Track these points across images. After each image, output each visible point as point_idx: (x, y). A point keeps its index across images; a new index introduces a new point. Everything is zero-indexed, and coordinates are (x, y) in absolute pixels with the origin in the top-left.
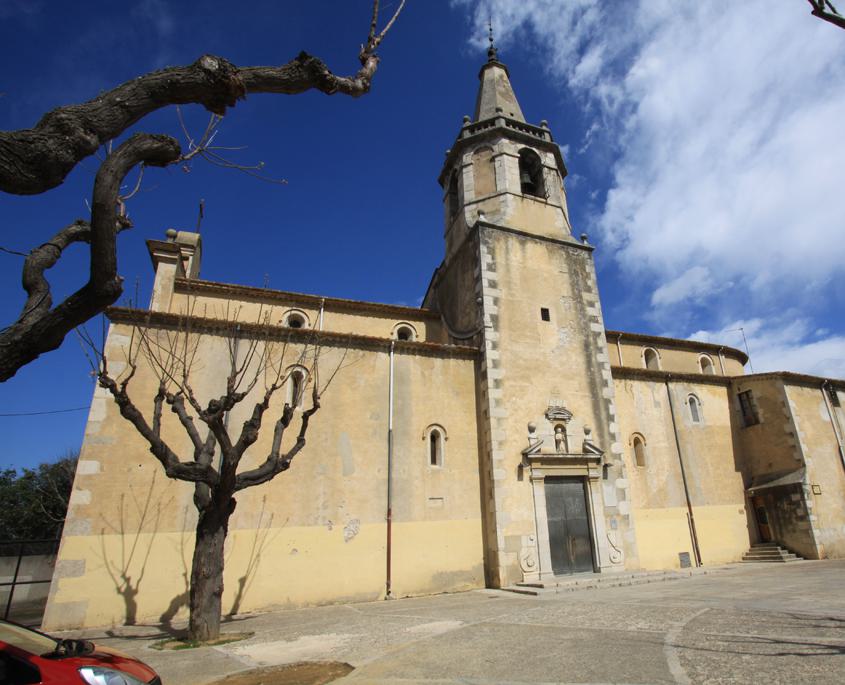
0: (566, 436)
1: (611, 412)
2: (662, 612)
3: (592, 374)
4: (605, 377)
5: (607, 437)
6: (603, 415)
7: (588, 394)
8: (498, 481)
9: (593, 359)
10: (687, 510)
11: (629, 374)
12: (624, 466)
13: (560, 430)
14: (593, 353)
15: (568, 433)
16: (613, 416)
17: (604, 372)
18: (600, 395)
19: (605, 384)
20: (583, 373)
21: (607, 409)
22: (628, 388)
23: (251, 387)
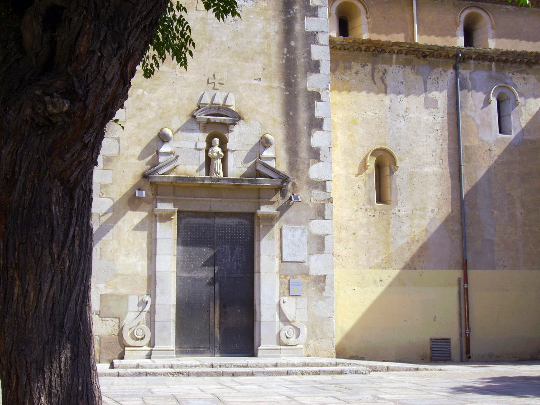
0: (225, 151)
1: (318, 114)
2: (107, 267)
3: (291, 50)
4: (315, 56)
5: (304, 154)
6: (303, 117)
7: (277, 84)
8: (174, 255)
9: (297, 27)
10: (458, 273)
11: (383, 51)
12: (330, 200)
13: (217, 141)
14: (299, 16)
15: (229, 146)
16: (322, 120)
17: (314, 49)
18: (301, 86)
19: (315, 67)
20: (274, 49)
21: (311, 108)
22: (377, 76)
23: (281, 395)
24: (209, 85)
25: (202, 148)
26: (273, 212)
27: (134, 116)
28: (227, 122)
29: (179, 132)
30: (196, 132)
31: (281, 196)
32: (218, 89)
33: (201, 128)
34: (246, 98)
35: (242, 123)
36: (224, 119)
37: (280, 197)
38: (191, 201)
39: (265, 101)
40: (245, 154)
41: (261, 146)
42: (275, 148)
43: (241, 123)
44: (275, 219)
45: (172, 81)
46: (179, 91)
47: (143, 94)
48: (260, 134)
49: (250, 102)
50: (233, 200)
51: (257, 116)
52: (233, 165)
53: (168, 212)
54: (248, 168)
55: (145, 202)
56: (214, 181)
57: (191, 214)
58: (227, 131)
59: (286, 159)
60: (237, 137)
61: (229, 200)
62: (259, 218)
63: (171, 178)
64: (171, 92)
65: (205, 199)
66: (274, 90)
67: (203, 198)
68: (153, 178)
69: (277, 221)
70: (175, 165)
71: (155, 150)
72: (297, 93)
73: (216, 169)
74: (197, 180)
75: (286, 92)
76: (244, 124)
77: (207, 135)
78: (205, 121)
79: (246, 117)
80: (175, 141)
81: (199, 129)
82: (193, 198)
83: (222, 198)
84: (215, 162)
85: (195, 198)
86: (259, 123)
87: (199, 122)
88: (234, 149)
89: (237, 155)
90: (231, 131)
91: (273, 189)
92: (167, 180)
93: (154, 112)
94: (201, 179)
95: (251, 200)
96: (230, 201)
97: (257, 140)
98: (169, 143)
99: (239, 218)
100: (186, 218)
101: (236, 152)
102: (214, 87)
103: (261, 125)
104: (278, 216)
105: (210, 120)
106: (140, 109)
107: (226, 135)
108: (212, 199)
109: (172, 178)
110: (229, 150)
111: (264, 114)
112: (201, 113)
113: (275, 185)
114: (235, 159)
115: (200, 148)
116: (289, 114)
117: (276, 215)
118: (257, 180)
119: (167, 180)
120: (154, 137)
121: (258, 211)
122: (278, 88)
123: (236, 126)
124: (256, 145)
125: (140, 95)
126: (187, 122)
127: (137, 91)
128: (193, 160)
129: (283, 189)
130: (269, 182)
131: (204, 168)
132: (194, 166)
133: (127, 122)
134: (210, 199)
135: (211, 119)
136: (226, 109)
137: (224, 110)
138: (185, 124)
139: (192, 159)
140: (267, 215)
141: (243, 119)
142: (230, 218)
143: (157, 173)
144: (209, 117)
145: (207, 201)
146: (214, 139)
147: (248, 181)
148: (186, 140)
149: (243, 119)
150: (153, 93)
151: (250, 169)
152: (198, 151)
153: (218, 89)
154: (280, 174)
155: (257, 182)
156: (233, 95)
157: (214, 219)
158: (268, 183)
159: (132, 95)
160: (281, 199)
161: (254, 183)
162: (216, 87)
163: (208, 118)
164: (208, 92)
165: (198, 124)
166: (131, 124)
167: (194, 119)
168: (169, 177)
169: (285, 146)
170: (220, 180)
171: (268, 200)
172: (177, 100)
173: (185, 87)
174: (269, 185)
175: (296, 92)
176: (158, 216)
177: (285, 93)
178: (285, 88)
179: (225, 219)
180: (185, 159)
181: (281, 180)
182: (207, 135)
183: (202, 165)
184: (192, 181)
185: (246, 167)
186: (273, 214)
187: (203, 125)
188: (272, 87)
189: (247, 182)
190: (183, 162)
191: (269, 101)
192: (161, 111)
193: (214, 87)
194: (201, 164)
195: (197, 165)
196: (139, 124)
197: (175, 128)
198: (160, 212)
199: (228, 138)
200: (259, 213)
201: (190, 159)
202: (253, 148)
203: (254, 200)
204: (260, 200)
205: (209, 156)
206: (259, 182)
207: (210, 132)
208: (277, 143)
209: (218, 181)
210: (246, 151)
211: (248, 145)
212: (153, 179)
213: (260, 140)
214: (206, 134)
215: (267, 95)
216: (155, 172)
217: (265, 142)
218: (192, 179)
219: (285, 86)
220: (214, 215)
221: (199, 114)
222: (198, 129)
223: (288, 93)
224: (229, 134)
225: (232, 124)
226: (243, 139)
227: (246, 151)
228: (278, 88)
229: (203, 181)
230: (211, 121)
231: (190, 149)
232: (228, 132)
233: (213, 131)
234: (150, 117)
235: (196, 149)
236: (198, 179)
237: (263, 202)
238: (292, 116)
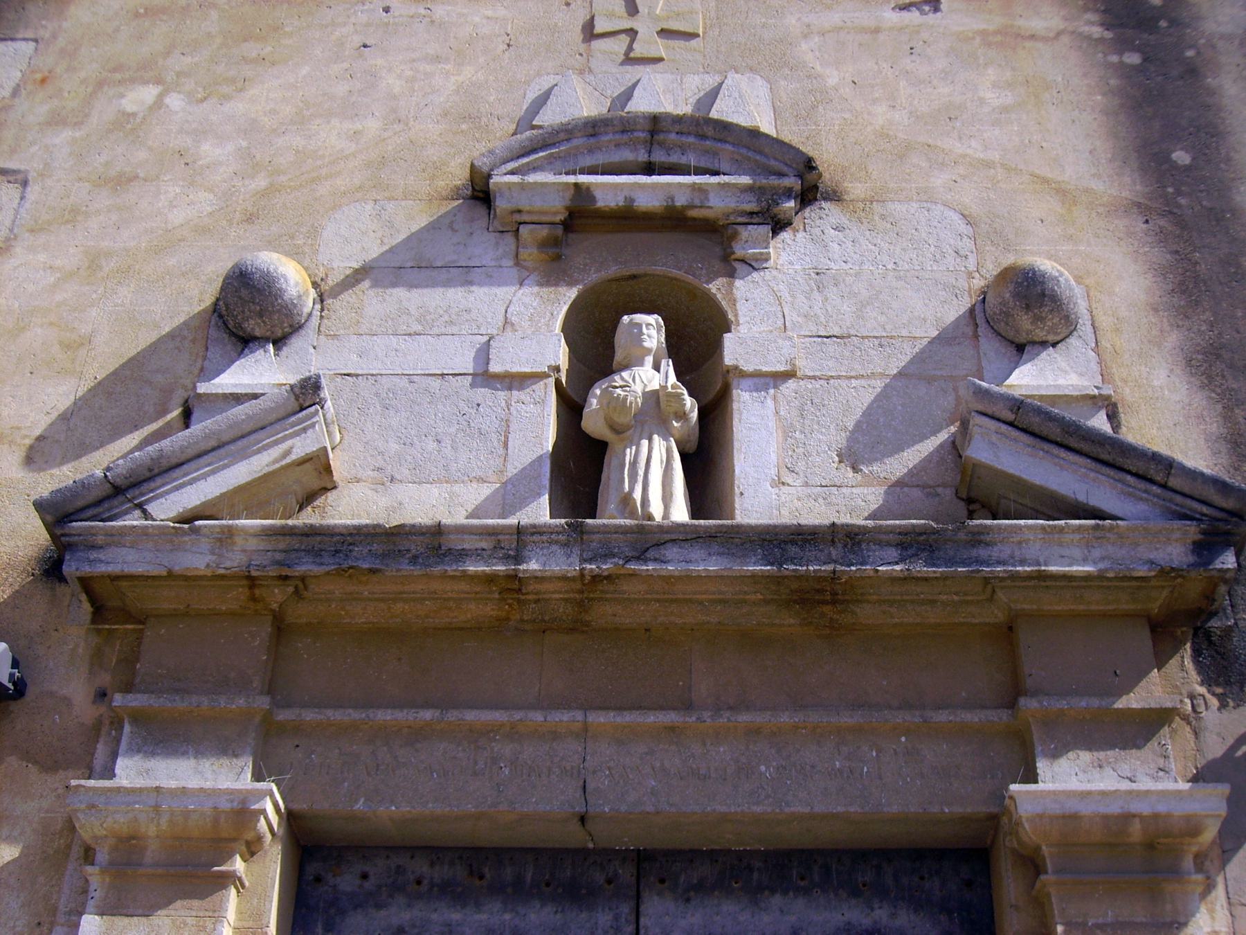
24: (597, 44)
25: (527, 369)
26: (1163, 794)
27: (73, 215)
28: (718, 205)
29: (366, 284)
30: (491, 279)
31: (1207, 681)
32: (661, 60)
33: (530, 254)
34: (847, 91)
35: (833, 221)
36: (693, 186)
37: (1202, 690)
38: (417, 735)
39: (982, 101)
40: (861, 396)
41: (989, 346)
42: (1097, 348)
43: (823, 217)
44: (1188, 863)
45: (358, 40)
46: (392, 82)
47: (159, 103)
48: (970, 276)
49: (881, 109)
50: (785, 718)
51: (939, 180)
52: (774, 471)
53: (187, 814)
54: (900, 483)
55: (27, 756)
56: (606, 556)
57: (425, 869)
58: (717, 265)
59: (1200, 417)
60: (801, 298)
61: (744, 718)
62: (1032, 864)
63: (239, 540)
64: (341, 89)
65: (538, 716)
66: (1040, 45)
67: (518, 715)
68: (94, 547)
69: (1209, 887)
70: (288, 453)
71: (179, 396)
72: (1198, 53)
73: (637, 495)
74: (462, 555)
75: (1121, 53)
76: (845, 221)
77: (572, 293)
78: (556, 206)
79: (855, 189)
80: (335, 336)
81: (517, 263)
82: (427, 715)
83: (687, 706)
84: (629, 454)
85: (452, 716)
86: (955, 217)
87: (518, 218)
88: (781, 368)
89: (801, 409)
90: (753, 264)
91: (1128, 616)
92: (209, 558)
93: (211, 190)
94: (498, 547)
95: (942, 717)
96: (754, 732)
97: (955, 310)
98: (285, 351)
99: (855, 893)
100: (379, 906)
101: (791, 384)
102: (630, 48)
103: (969, 223)
104: (1210, 834)
105: (593, 199)
106: (121, 182)
107: (715, 287)
108: (599, 718)
109: (253, 544)
110: (743, 375)
111: (989, 165)
112: (525, 160)
113: (1142, 571)
114: (787, 431)
115: (516, 369)
116: (1167, 159)
117: (1192, 828)
118: (977, 539)
119: (209, 558)
120: (181, 319)
121: (1014, 787)
122: (1065, 39)
123: (785, 235)
124: (945, 338)
125: (134, 115)
126: (432, 227)
127: (122, 96)
128: (454, 448)
129: (1215, 623)
130: (1089, 546)
131: (539, 495)
132: (457, 488)
133: (18, 250)
134: (579, 715)
135: (598, 194)
136: (709, 131)
137: (691, 139)
138: (414, 239)
139: (447, 442)
140: (1106, 818)
141: (835, 196)
142: (777, 900)
143: (137, 513)
144: (583, 179)
145: (555, 736)
146: (626, 319)
147: (901, 546)
148: (417, 327)
149: (835, 196)
150: (226, 98)
151: (916, 493)
152: (502, 395)
153: (661, 60)
154: (1174, 482)
155: (983, 552)
156: (760, 81)
157: (626, 909)
158: (1077, 553)
159: (87, 116)
160: (1214, 702)
161: (951, 562)
162: (639, 50)
163: (576, 185)
164: (590, 78)
165: (509, 238)
166: (42, 257)
167: (481, 210)
168: (230, 532)
169: (1173, 339)
170: (658, 545)
171: (1095, 702)
172: (372, 126)
173: (437, 59)
174: (1088, 568)
175: (1190, 53)
176: (102, 856)
177: (1114, 59)
178: (1108, 35)
179: (729, 907)
180: (394, 446)
181: (1192, 531)
182: (571, 294)
183: (527, 473)
184: (414, 560)
185: (880, 481)
186: (1161, 808)
187: (544, 232)
188: (1018, 35)
189: (893, 553)
190: (380, 462)
191: (1008, 98)
192: (261, 182)
193: (630, 48)
194: (511, 471)
195: (481, 480)
196: (94, 261)
197: (341, 260)
198: (119, 821)
199: (734, 302)
200: (1025, 809)
201: (431, 445)
202: (919, 359)
203: (972, 717)
204: (1028, 704)
205: (584, 433)
206: (995, 553)
207: (594, 277)
208: (1104, 321)
209: (641, 557)
210: (872, 376)
211: (882, 342)
212: (94, 555)
213: (972, 311)
214: (562, 289)
215: (990, 71)
216: (118, 504)
217: (1017, 295)
218: (416, 546)
219: (1107, 26)
220: (626, 874)
221: (512, 165)
222: (509, 262)
223: (1133, 59)
224: (738, 283)
225: (754, 217)
226: (847, 308)
227: (872, 376)
228: (1065, 39)
229: (506, 558)
230: (600, 204)
231: (436, 383)
232: (731, 274)
233: (613, 271)
234: (177, 217)
235: (484, 377)
236: (469, 543)
237: (1051, 723)
238: (1187, 168)
